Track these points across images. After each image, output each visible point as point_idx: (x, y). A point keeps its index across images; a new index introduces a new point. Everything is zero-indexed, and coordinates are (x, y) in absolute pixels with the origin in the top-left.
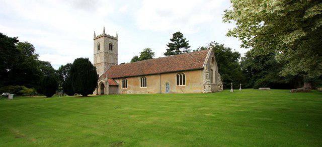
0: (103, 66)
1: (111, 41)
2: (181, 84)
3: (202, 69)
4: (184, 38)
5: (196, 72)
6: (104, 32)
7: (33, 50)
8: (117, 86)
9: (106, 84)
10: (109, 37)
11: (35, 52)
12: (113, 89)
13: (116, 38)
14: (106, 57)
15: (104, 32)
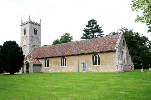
0: (28, 48)
1: (35, 27)
3: (115, 51)
5: (109, 53)
6: (30, 19)
8: (41, 65)
12: (37, 67)
15: (30, 19)
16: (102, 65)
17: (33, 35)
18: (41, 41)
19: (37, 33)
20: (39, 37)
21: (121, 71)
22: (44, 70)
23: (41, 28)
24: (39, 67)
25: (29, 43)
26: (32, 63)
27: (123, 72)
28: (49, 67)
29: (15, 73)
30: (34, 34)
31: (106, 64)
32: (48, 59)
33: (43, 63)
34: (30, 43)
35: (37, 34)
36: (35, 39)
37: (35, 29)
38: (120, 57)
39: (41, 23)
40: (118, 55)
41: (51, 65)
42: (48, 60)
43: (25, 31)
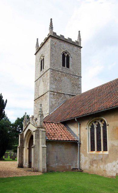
0: (48, 99)
2: (99, 149)
6: (51, 27)
8: (75, 144)
9: (38, 136)
10: (61, 39)
12: (60, 152)
13: (77, 42)
14: (55, 80)
15: (51, 27)
17: (60, 67)
18: (80, 84)
19: (71, 63)
20: (77, 74)
22: (85, 163)
25: (48, 89)
26: (41, 133)
28: (107, 153)
30: (64, 65)
32: (102, 121)
33: (82, 135)
34: (50, 88)
35: (70, 66)
36: (64, 79)
37: (66, 55)
39: (80, 39)
41: (116, 143)
42: (102, 125)
43: (41, 61)
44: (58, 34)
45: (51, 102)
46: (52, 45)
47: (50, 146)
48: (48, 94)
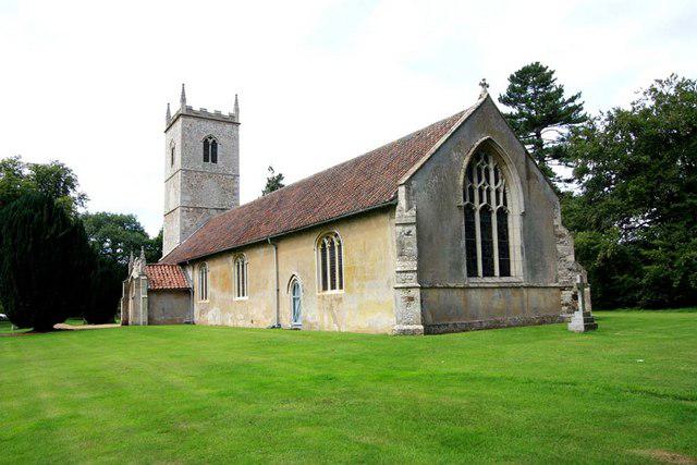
1: (210, 129)
2: (333, 287)
3: (389, 208)
4: (509, 83)
5: (373, 222)
6: (183, 100)
7: (70, 183)
10: (202, 116)
11: (79, 190)
12: (164, 302)
15: (183, 100)
16: (350, 291)
17: (200, 165)
18: (237, 189)
19: (219, 153)
21: (405, 327)
23: (240, 133)
24: (179, 300)
27: (414, 333)
29: (55, 326)
30: (206, 160)
31: (363, 286)
36: (208, 183)
37: (211, 141)
38: (413, 239)
39: (237, 110)
40: (400, 228)
44: (196, 108)
45: (182, 224)
46: (183, 129)
47: (248, 286)
48: (178, 211)
